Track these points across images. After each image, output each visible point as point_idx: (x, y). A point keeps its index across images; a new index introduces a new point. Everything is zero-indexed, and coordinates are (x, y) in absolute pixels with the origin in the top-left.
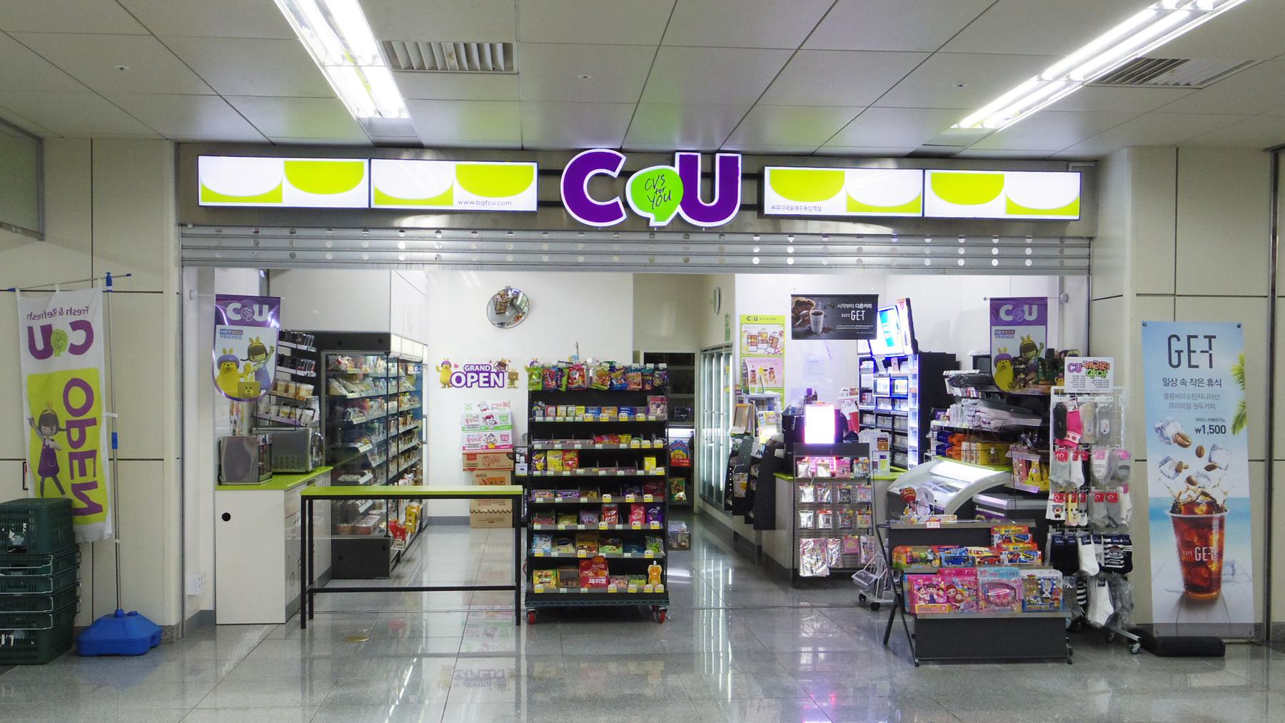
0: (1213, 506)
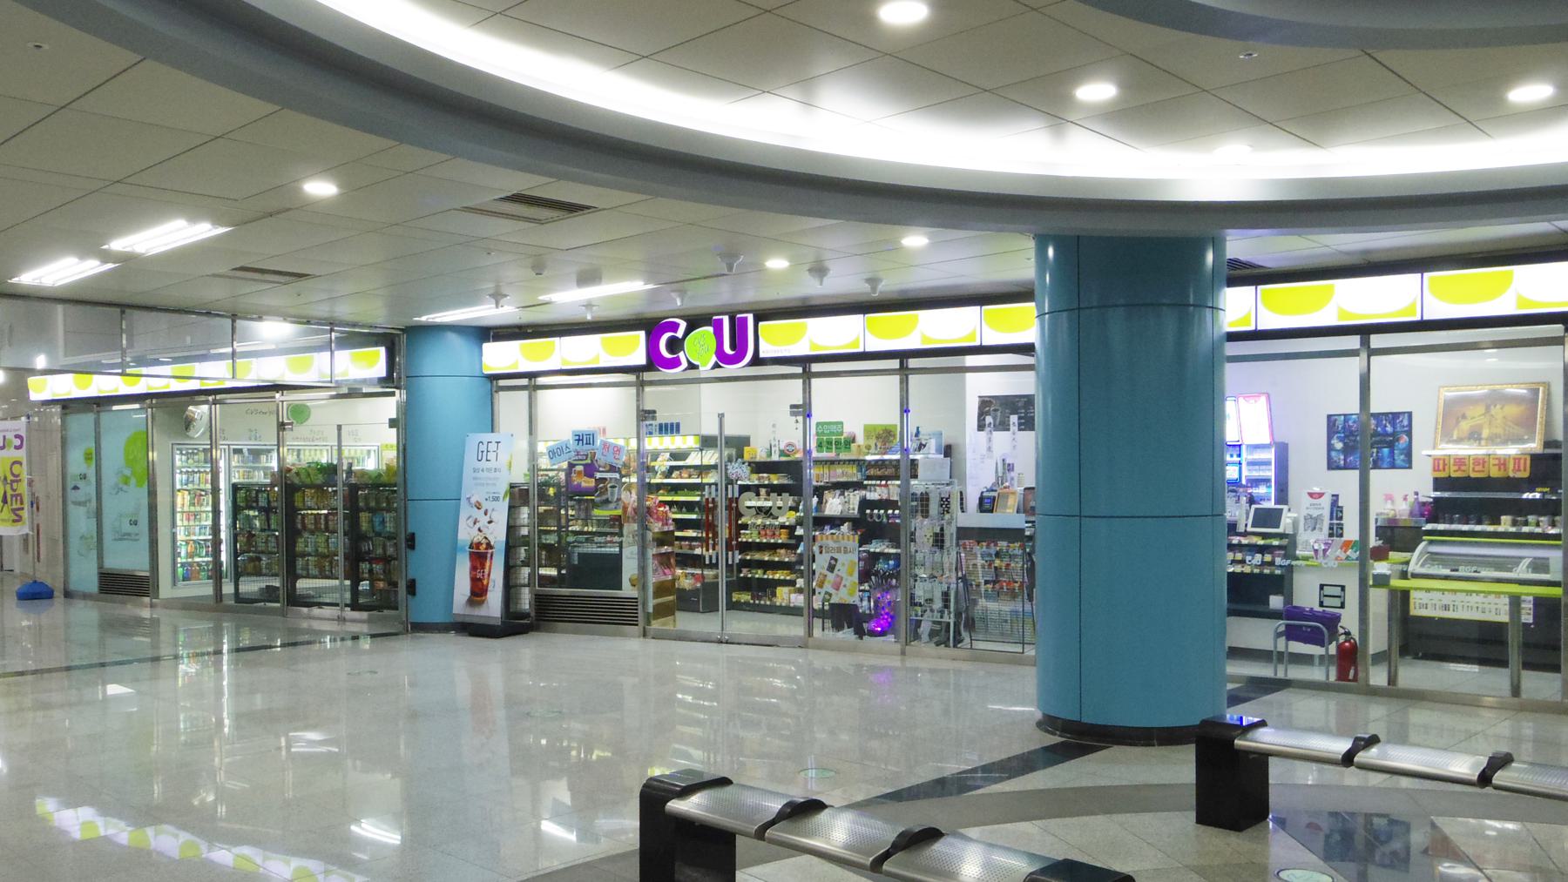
0: (489, 546)
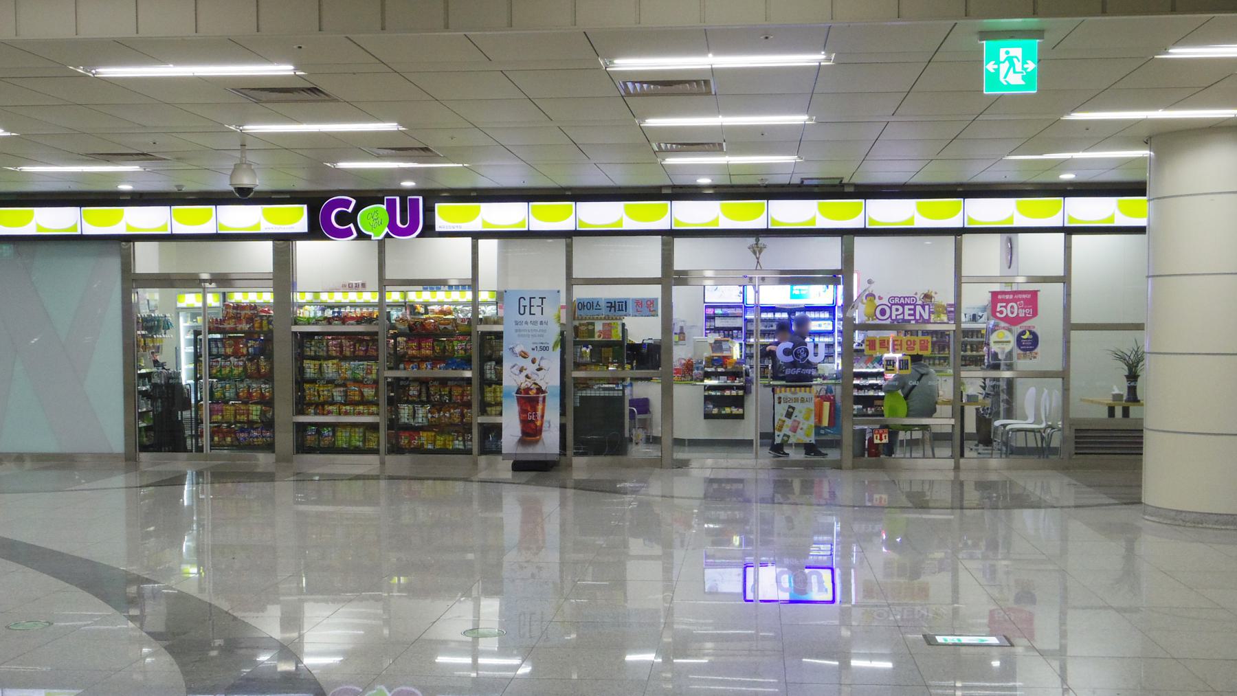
0: (540, 390)
